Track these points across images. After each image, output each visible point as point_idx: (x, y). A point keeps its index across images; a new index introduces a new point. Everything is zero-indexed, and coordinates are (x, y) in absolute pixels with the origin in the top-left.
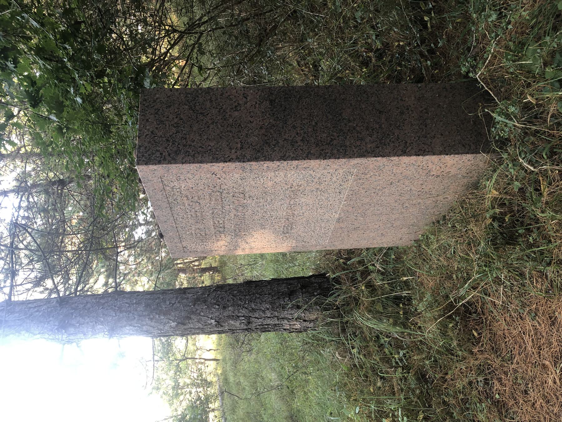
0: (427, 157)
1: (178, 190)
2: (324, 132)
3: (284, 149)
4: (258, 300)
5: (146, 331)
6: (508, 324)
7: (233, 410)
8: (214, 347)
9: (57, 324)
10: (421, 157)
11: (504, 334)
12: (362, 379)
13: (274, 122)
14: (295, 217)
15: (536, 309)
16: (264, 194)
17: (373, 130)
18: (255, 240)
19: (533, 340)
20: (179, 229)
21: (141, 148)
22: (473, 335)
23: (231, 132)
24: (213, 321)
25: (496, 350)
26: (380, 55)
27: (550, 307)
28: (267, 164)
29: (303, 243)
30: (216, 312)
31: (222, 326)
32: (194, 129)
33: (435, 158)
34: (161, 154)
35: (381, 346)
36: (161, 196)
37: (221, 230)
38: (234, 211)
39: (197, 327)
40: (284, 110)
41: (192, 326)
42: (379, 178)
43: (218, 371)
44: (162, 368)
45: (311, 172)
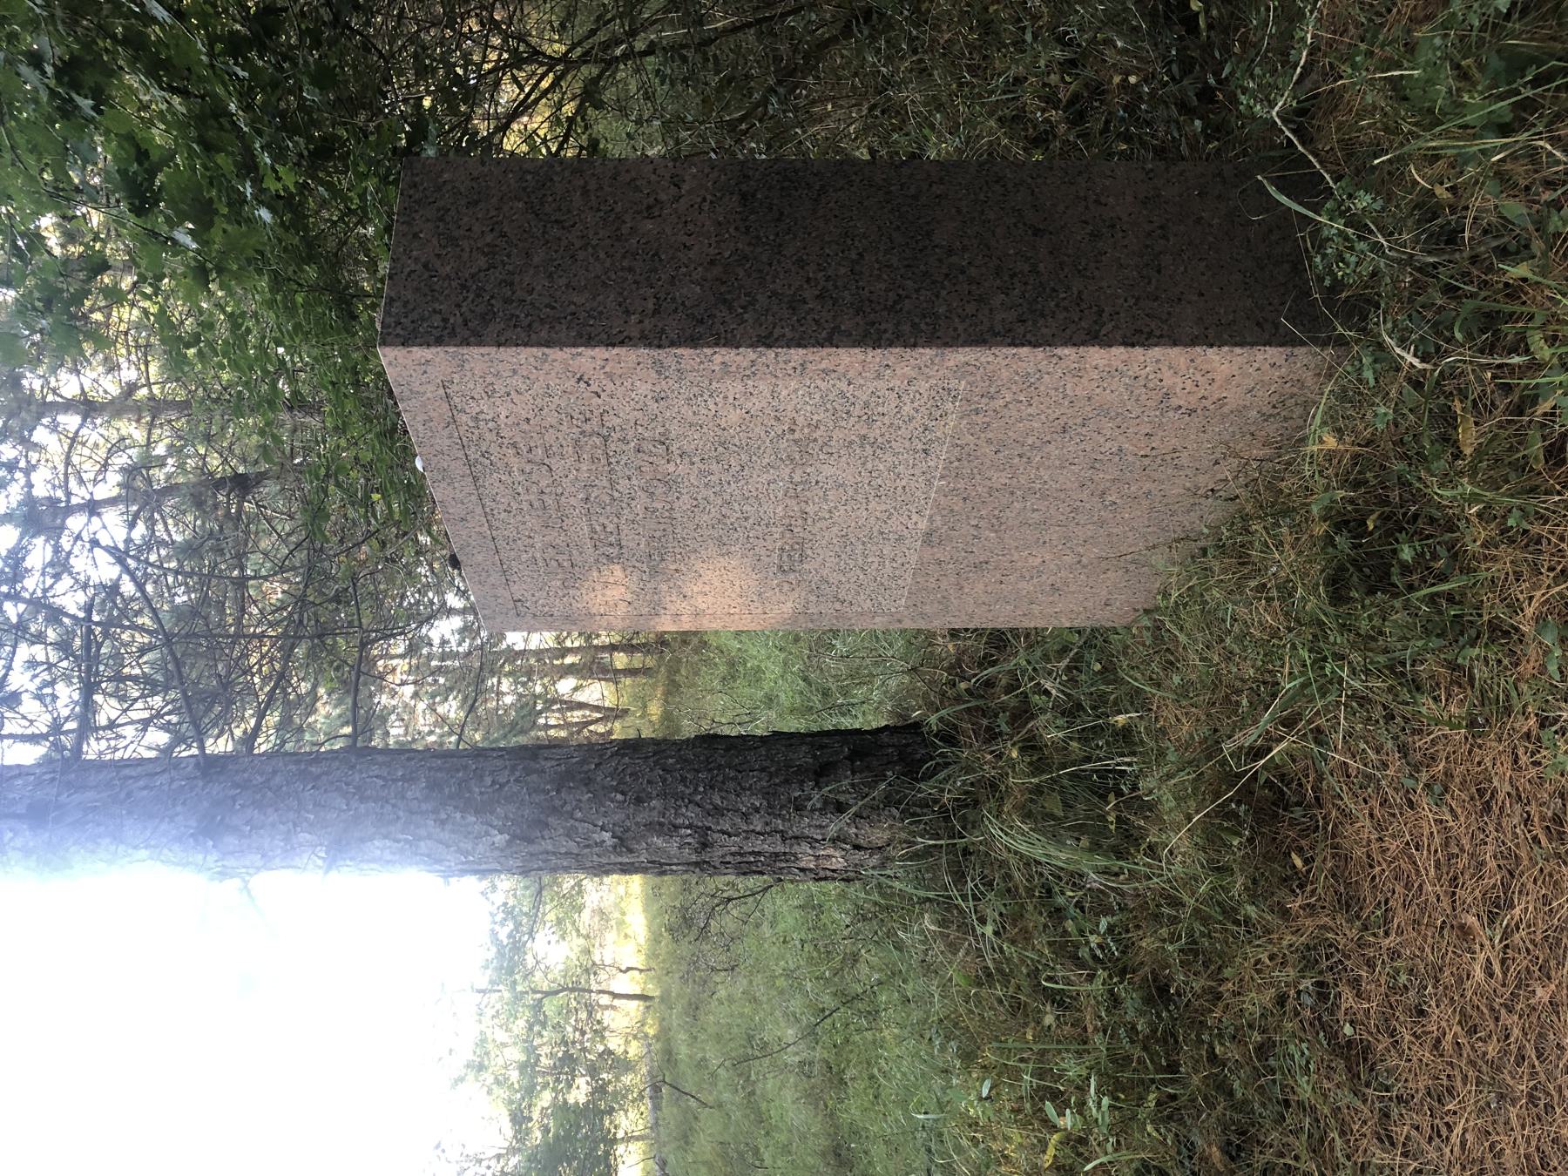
0: (1156, 352)
1: (491, 425)
2: (879, 277)
3: (770, 318)
4: (731, 785)
5: (428, 856)
6: (1379, 827)
7: (685, 1139)
8: (639, 961)
9: (193, 823)
10: (1138, 350)
11: (1369, 856)
12: (1010, 1011)
13: (748, 249)
14: (810, 521)
15: (1446, 774)
16: (720, 449)
17: (1012, 277)
18: (707, 588)
19: (1437, 862)
20: (501, 543)
21: (396, 304)
22: (1294, 866)
23: (630, 269)
24: (607, 836)
25: (1348, 903)
26: (1077, 113)
27: (1479, 764)
28: (723, 355)
29: (838, 606)
30: (616, 811)
31: (631, 851)
32: (536, 260)
33: (1178, 356)
34: (445, 320)
35: (1058, 914)
36: (447, 442)
37: (614, 551)
38: (644, 495)
39: (563, 850)
40: (778, 220)
41: (550, 848)
42: (1030, 410)
43: (646, 1029)
44: (493, 1012)
45: (843, 385)
